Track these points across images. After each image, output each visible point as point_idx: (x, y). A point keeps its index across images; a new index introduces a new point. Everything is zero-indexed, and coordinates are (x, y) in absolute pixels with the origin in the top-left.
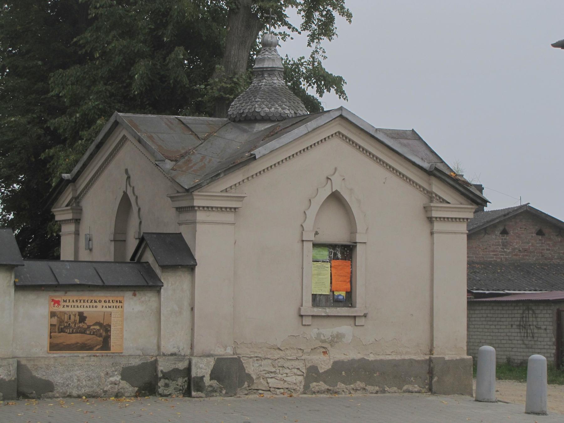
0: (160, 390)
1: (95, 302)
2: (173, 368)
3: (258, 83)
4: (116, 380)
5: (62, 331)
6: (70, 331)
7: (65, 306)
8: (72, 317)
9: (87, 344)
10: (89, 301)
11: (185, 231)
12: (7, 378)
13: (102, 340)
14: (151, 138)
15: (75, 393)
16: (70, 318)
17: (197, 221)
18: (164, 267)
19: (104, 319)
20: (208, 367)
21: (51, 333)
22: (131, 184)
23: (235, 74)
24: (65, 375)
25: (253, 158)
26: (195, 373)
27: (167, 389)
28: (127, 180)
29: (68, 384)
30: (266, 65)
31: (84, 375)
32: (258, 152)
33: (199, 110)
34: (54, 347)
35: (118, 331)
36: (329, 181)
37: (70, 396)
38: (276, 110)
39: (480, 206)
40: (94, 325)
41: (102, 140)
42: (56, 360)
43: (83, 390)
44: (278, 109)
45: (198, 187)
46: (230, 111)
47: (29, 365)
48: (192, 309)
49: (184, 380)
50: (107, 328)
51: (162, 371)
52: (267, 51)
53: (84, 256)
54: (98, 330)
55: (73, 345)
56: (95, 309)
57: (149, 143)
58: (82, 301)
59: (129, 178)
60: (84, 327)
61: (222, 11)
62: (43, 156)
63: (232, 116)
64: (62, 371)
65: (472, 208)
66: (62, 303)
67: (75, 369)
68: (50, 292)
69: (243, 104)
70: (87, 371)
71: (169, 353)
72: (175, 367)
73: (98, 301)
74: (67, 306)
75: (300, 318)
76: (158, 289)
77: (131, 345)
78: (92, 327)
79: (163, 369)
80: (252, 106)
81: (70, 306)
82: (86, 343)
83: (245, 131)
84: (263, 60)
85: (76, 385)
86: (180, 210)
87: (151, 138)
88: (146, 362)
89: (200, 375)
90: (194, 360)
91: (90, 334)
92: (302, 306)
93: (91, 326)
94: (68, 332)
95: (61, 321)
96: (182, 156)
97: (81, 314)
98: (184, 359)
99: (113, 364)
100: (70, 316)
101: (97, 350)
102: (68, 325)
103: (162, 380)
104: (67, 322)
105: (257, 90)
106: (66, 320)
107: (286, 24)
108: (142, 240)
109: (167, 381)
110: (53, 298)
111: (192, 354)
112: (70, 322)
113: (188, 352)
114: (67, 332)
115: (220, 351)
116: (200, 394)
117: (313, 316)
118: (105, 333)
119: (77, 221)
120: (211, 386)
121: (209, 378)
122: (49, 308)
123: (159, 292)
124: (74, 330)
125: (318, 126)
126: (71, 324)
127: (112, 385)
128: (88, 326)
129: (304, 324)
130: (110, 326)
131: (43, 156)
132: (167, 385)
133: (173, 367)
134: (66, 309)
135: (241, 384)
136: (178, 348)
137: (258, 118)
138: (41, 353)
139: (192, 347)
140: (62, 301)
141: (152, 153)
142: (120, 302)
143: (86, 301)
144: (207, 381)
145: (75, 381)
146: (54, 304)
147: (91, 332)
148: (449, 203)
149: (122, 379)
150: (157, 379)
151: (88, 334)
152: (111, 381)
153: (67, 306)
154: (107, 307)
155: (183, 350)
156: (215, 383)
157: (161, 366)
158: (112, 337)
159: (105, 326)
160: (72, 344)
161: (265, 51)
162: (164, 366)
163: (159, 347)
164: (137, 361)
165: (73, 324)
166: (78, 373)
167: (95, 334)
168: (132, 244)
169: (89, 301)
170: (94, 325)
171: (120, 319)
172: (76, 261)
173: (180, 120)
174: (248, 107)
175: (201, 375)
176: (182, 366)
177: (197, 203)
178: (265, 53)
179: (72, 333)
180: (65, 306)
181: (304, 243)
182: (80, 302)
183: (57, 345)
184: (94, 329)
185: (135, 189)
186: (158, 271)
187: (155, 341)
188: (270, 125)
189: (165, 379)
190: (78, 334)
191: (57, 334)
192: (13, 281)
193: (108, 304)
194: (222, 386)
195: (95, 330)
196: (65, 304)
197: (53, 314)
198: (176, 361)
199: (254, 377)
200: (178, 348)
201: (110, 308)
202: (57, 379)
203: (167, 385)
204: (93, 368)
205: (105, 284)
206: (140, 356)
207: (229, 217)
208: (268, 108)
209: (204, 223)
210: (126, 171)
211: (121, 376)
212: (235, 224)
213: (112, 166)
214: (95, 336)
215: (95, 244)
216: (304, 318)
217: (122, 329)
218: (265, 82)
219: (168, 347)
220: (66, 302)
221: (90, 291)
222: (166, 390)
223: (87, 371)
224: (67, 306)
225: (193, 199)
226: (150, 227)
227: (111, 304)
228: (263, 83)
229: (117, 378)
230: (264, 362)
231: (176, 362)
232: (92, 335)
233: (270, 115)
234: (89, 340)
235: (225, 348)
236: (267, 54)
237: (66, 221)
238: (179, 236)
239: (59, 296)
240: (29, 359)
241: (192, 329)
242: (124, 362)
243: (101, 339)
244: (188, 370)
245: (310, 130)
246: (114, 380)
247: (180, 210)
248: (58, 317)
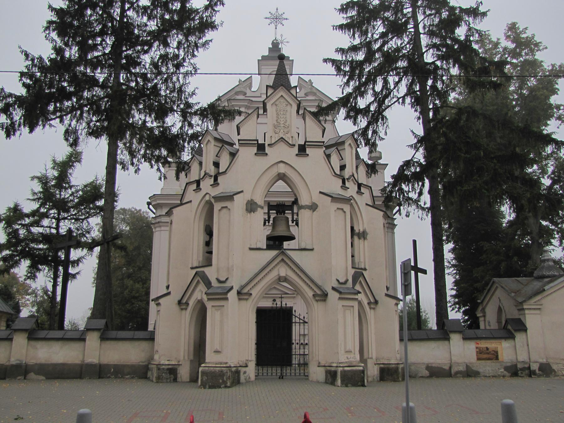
0: (520, 375)
5: (480, 353)
11: (522, 317)
12: (463, 370)
14: (506, 286)
15: (488, 375)
18: (516, 330)
23: (536, 263)
25: (544, 290)
26: (532, 368)
30: (546, 258)
32: (546, 288)
33: (525, 276)
34: (478, 359)
37: (486, 376)
45: (525, 301)
46: (534, 275)
47: (471, 366)
48: (528, 345)
50: (497, 352)
53: (488, 327)
57: (505, 287)
59: (500, 300)
61: (104, 6)
62: (473, 296)
83: (540, 281)
84: (544, 256)
86: (519, 310)
87: (506, 286)
90: (531, 364)
95: (480, 350)
96: (518, 291)
105: (543, 267)
107: (553, 245)
108: (506, 321)
111: (530, 362)
113: (528, 361)
115: (541, 361)
116: (535, 376)
119: (484, 316)
120: (539, 373)
123: (514, 339)
130: (498, 352)
131: (473, 296)
132: (522, 373)
133: (523, 366)
134: (481, 346)
135: (551, 373)
139: (530, 359)
141: (507, 291)
144: (537, 372)
156: (540, 372)
162: (519, 366)
163: (517, 359)
166: (488, 368)
168: (504, 322)
172: (485, 329)
173: (518, 281)
176: (526, 366)
177: (525, 307)
186: (513, 332)
187: (515, 357)
197: (477, 348)
199: (556, 370)
202: (481, 370)
207: (538, 312)
209: (528, 314)
210: (499, 298)
213: (494, 297)
215: (491, 324)
217: (502, 353)
218: (546, 264)
219: (520, 359)
226: (509, 317)
229: (502, 370)
230: (559, 365)
235: (543, 359)
236: (545, 254)
237: (481, 317)
238: (520, 319)
239: (478, 341)
240: (470, 363)
241: (529, 353)
242: (504, 365)
243: (495, 356)
244: (529, 368)
247: (519, 310)
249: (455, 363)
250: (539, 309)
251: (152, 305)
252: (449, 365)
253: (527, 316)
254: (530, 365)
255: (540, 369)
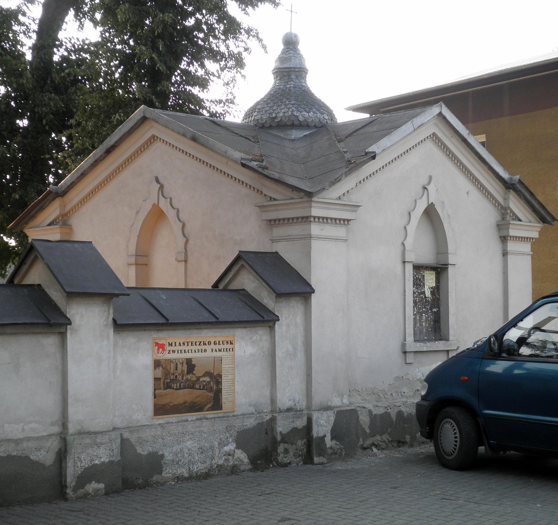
0: (281, 458)
1: (205, 344)
2: (291, 428)
3: (285, 85)
4: (231, 449)
5: (168, 386)
6: (177, 386)
7: (171, 352)
8: (179, 366)
9: (196, 403)
10: (198, 344)
13: (213, 396)
16: (176, 369)
17: (312, 236)
19: (214, 367)
20: (329, 423)
21: (155, 390)
22: (165, 195)
24: (174, 449)
26: (317, 432)
27: (286, 456)
28: (159, 190)
29: (178, 461)
31: (195, 446)
35: (229, 383)
36: (426, 190)
38: (315, 115)
39: (546, 225)
40: (204, 375)
41: (116, 142)
42: (164, 428)
43: (196, 468)
44: (317, 113)
47: (133, 438)
49: (303, 442)
50: (217, 379)
51: (281, 433)
52: (291, 49)
54: (209, 382)
55: (181, 405)
56: (203, 354)
58: (190, 344)
59: (162, 187)
60: (192, 379)
63: (260, 121)
64: (170, 444)
65: (539, 227)
66: (168, 348)
67: (186, 439)
68: (153, 332)
69: (275, 108)
70: (199, 440)
71: (286, 408)
72: (293, 427)
73: (207, 343)
74: (172, 351)
75: (403, 355)
76: (271, 324)
77: (243, 400)
78: (201, 379)
79: (282, 430)
80: (288, 110)
81: (176, 352)
82: (195, 401)
85: (187, 461)
88: (261, 421)
89: (321, 434)
90: (315, 415)
91: (200, 389)
92: (405, 340)
93: (200, 377)
94: (175, 388)
95: (167, 373)
97: (189, 361)
98: (301, 414)
99: (227, 427)
100: (177, 364)
101: (208, 410)
102: (174, 378)
103: (282, 445)
104: (173, 374)
106: (172, 371)
109: (286, 446)
110: (156, 341)
111: (309, 407)
112: (176, 374)
114: (173, 388)
115: (336, 402)
117: (416, 352)
118: (216, 386)
121: (330, 438)
122: (153, 354)
124: (182, 385)
125: (422, 124)
126: (178, 377)
127: (225, 457)
128: (196, 377)
129: (407, 362)
130: (220, 376)
133: (292, 426)
136: (294, 401)
137: (296, 123)
138: (144, 420)
140: (168, 343)
142: (231, 343)
143: (194, 343)
144: (329, 442)
145: (186, 455)
146: (158, 349)
147: (200, 386)
148: (520, 220)
149: (237, 447)
150: (275, 443)
151: (197, 389)
152: (225, 451)
153: (172, 351)
154: (218, 350)
155: (299, 402)
157: (280, 426)
158: (223, 391)
159: (215, 377)
160: (179, 404)
161: (289, 50)
163: (273, 401)
164: (252, 421)
165: (181, 377)
167: (205, 388)
169: (198, 344)
170: (204, 375)
171: (231, 366)
174: (283, 111)
175: (322, 435)
176: (301, 423)
177: (316, 212)
178: (290, 52)
179: (180, 389)
180: (171, 352)
181: (406, 264)
182: (188, 345)
183: (164, 406)
184: (204, 381)
185: (173, 201)
187: (267, 393)
188: (309, 132)
189: (284, 443)
190: (186, 390)
191: (162, 391)
192: (112, 318)
193: (217, 347)
194: (343, 447)
195: (205, 383)
196: (171, 348)
197: (157, 364)
198: (294, 417)
200: (294, 401)
201: (220, 352)
203: (286, 451)
204: (205, 435)
205: (219, 320)
206: (252, 414)
207: (339, 231)
208: (307, 113)
209: (319, 238)
211: (236, 444)
212: (347, 240)
214: (205, 391)
216: (407, 354)
220: (172, 346)
221: (185, 329)
222: (286, 457)
223: (199, 440)
224: (174, 352)
225: (311, 207)
227: (221, 347)
228: (292, 85)
229: (231, 447)
231: (295, 420)
232: (202, 390)
233: (309, 121)
234: (198, 397)
239: (165, 337)
240: (131, 429)
242: (238, 424)
243: (211, 394)
245: (416, 127)
246: (229, 450)
248: (163, 368)
249: (81, 433)
250: (346, 222)
251: (451, 355)
252: (54, 445)
253: (315, 245)
254: (310, 420)
255: (336, 434)
